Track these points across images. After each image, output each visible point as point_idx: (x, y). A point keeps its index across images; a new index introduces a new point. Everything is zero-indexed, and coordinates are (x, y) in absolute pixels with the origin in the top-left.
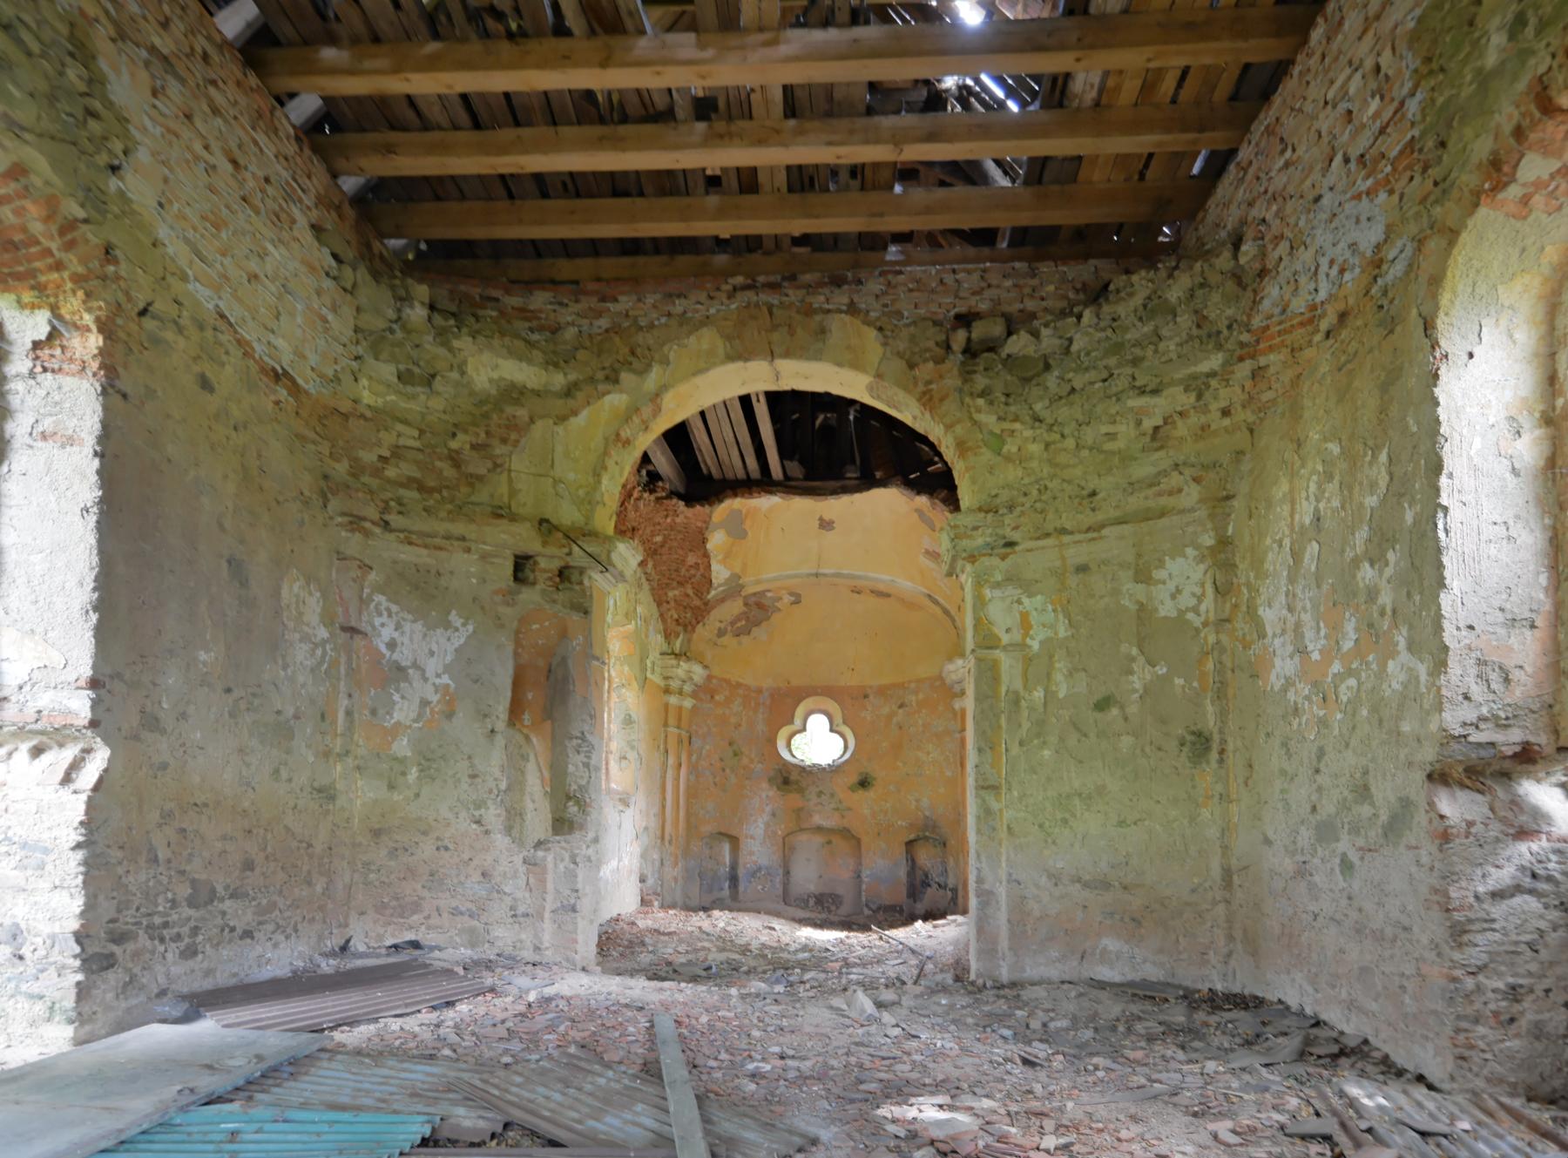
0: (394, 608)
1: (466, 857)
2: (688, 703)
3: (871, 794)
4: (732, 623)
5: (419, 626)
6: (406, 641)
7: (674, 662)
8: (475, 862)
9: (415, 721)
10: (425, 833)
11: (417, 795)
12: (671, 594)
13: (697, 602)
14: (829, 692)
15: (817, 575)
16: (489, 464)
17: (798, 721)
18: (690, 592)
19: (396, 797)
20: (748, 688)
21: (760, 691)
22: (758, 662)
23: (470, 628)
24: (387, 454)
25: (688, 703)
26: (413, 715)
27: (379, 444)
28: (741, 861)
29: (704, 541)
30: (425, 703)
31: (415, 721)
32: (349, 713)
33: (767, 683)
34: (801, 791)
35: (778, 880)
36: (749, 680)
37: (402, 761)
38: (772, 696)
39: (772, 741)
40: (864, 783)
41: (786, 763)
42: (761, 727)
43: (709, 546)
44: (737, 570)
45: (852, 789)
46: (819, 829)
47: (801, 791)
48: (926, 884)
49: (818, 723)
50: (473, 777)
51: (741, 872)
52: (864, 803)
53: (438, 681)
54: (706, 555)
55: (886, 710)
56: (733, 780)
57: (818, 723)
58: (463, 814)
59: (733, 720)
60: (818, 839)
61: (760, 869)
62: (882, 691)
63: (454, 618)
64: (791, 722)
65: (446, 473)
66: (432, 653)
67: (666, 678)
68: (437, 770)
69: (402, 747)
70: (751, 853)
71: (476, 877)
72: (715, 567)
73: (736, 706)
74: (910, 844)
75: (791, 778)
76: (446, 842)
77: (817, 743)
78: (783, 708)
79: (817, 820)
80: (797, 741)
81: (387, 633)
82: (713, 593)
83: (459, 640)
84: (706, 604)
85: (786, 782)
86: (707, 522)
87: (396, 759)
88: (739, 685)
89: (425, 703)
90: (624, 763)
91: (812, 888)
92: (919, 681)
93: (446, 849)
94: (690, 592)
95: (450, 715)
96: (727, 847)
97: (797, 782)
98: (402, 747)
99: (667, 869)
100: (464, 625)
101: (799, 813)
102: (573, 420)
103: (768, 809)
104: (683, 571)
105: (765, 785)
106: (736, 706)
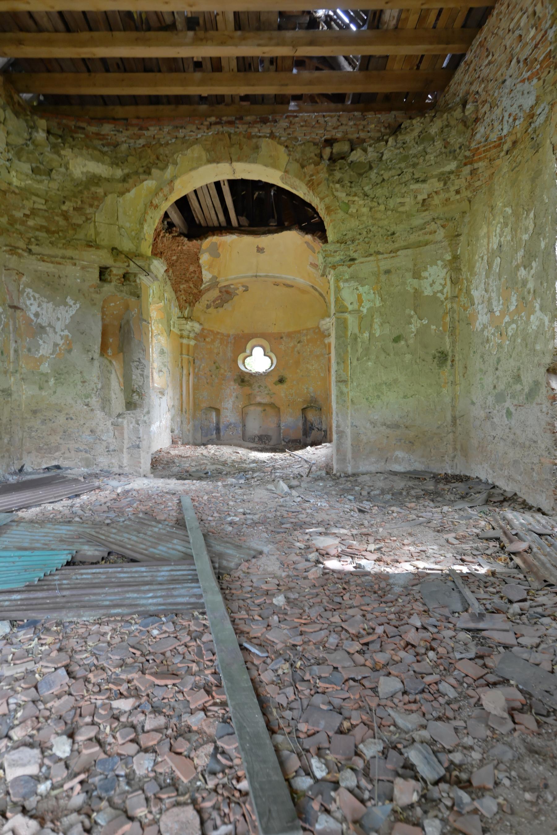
0: (37, 296)
1: (82, 423)
2: (192, 343)
3: (284, 386)
4: (214, 302)
5: (50, 305)
6: (44, 312)
7: (185, 322)
8: (87, 425)
9: (51, 354)
10: (60, 411)
11: (55, 392)
12: (182, 287)
13: (195, 291)
14: (263, 336)
15: (256, 276)
16: (84, 219)
17: (248, 351)
18: (192, 286)
19: (44, 393)
20: (222, 334)
21: (228, 336)
22: (227, 321)
23: (78, 305)
24: (28, 212)
25: (192, 343)
26: (50, 351)
27: (23, 207)
28: (221, 420)
29: (198, 259)
30: (56, 345)
31: (51, 354)
32: (16, 351)
33: (232, 332)
34: (250, 385)
35: (240, 429)
36: (223, 330)
37: (46, 375)
38: (235, 338)
39: (235, 361)
40: (281, 381)
41: (242, 372)
42: (229, 354)
43: (201, 261)
44: (216, 274)
45: (275, 384)
46: (260, 404)
47: (250, 385)
48: (312, 429)
49: (258, 352)
50: (84, 382)
51: (221, 426)
52: (282, 391)
53: (62, 333)
54: (199, 266)
55: (291, 345)
56: (216, 381)
57: (258, 352)
58: (79, 401)
59: (215, 351)
60: (259, 409)
61: (230, 424)
62: (290, 335)
63: (69, 300)
64: (244, 351)
65: (60, 223)
66: (58, 319)
67: (181, 330)
68: (65, 379)
69: (45, 368)
70: (226, 417)
71: (88, 432)
72: (204, 272)
73: (217, 343)
74: (304, 410)
75: (245, 379)
76: (71, 415)
77: (258, 361)
78: (241, 344)
79: (259, 399)
80: (248, 361)
81: (34, 309)
82: (203, 286)
83: (72, 312)
84: (200, 292)
85: (243, 381)
86: (199, 249)
87: (42, 374)
88: (218, 333)
89: (56, 345)
90: (161, 374)
91: (257, 432)
92: (308, 330)
93: (72, 419)
94: (192, 286)
95: (69, 351)
96: (214, 414)
97: (248, 381)
98: (45, 368)
99: (185, 425)
100: (75, 304)
101: (249, 396)
102: (127, 194)
103: (234, 395)
104: (188, 275)
105: (232, 383)
106: (217, 343)
